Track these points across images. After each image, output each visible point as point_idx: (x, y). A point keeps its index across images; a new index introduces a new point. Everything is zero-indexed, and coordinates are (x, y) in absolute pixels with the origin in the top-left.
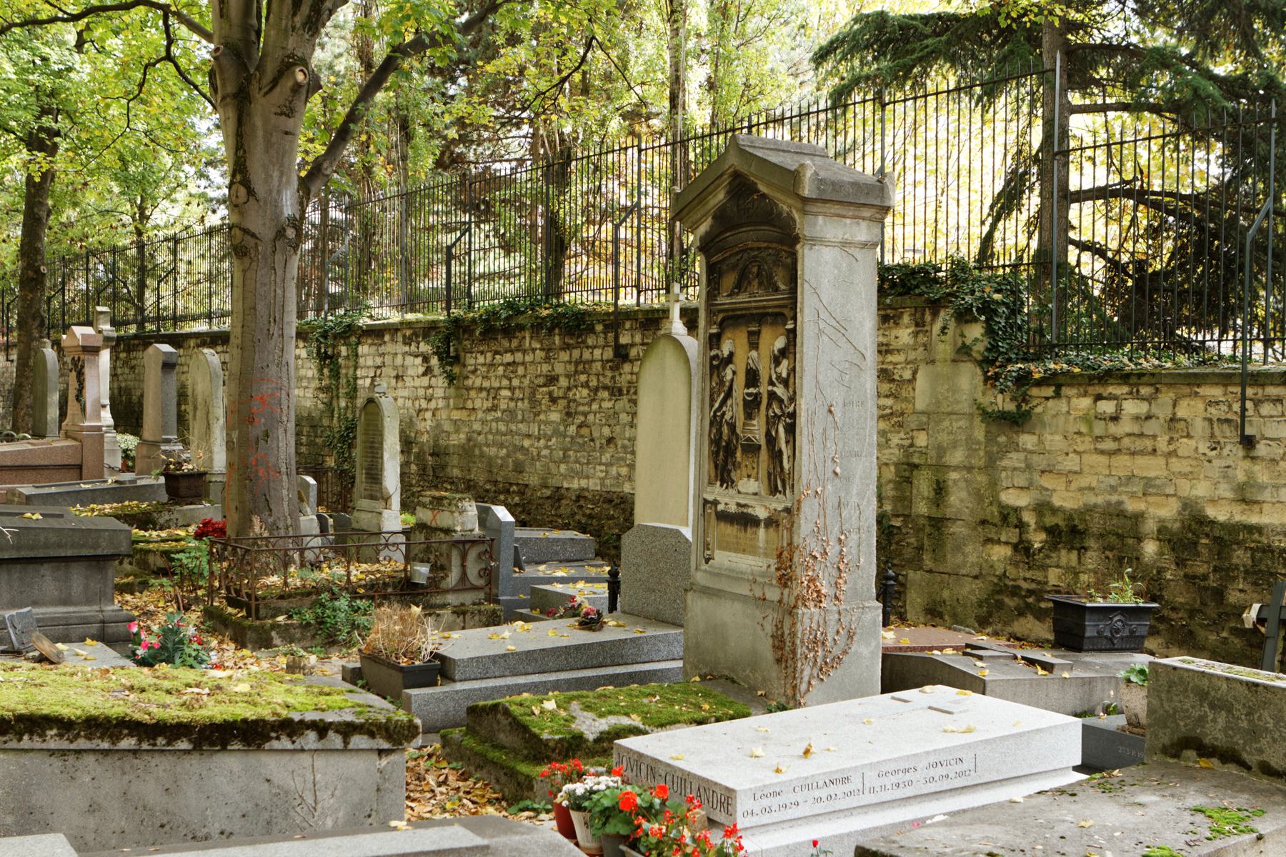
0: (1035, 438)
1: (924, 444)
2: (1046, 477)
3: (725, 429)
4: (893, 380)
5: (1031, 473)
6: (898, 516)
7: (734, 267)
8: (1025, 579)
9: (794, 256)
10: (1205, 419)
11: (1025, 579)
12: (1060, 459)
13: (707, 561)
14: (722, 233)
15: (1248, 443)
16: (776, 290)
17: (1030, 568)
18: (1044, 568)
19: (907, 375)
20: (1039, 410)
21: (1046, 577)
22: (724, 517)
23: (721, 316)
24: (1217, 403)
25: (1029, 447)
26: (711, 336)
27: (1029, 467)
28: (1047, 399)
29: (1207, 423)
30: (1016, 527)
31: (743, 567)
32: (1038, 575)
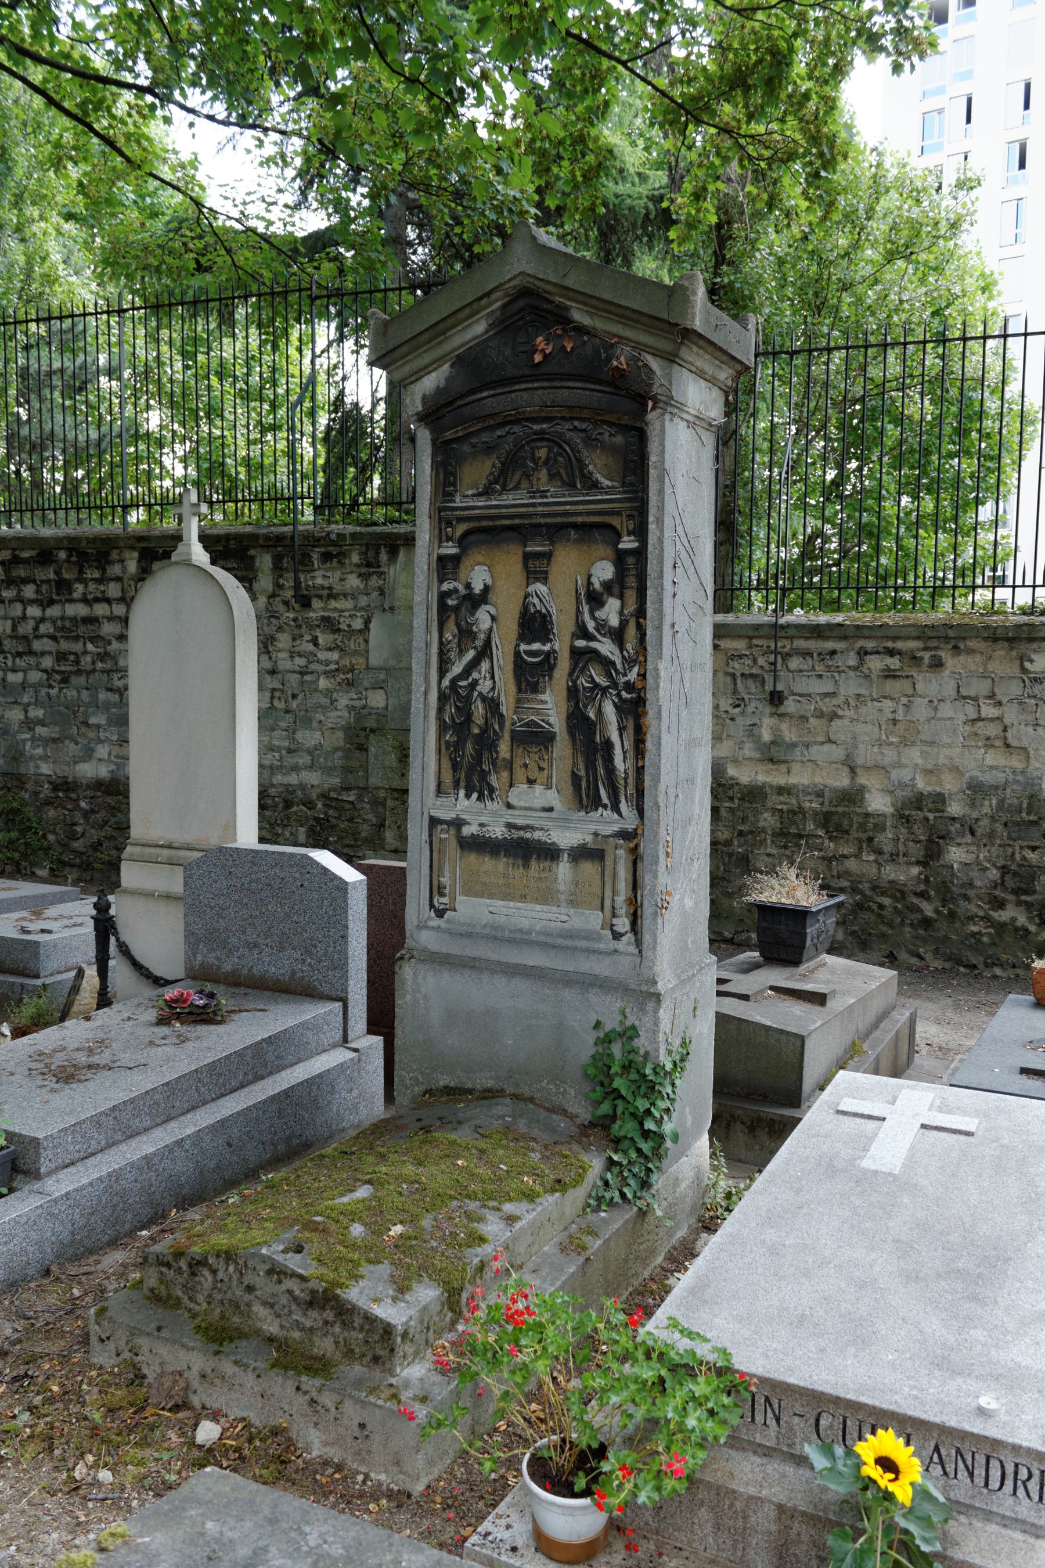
1: (382, 704)
3: (479, 710)
4: (339, 630)
6: (348, 789)
7: (489, 449)
9: (641, 437)
10: (727, 674)
13: (440, 914)
14: (473, 391)
15: (776, 698)
16: (595, 485)
19: (358, 624)
22: (479, 845)
23: (461, 529)
24: (740, 657)
26: (441, 559)
29: (729, 679)
31: (525, 924)
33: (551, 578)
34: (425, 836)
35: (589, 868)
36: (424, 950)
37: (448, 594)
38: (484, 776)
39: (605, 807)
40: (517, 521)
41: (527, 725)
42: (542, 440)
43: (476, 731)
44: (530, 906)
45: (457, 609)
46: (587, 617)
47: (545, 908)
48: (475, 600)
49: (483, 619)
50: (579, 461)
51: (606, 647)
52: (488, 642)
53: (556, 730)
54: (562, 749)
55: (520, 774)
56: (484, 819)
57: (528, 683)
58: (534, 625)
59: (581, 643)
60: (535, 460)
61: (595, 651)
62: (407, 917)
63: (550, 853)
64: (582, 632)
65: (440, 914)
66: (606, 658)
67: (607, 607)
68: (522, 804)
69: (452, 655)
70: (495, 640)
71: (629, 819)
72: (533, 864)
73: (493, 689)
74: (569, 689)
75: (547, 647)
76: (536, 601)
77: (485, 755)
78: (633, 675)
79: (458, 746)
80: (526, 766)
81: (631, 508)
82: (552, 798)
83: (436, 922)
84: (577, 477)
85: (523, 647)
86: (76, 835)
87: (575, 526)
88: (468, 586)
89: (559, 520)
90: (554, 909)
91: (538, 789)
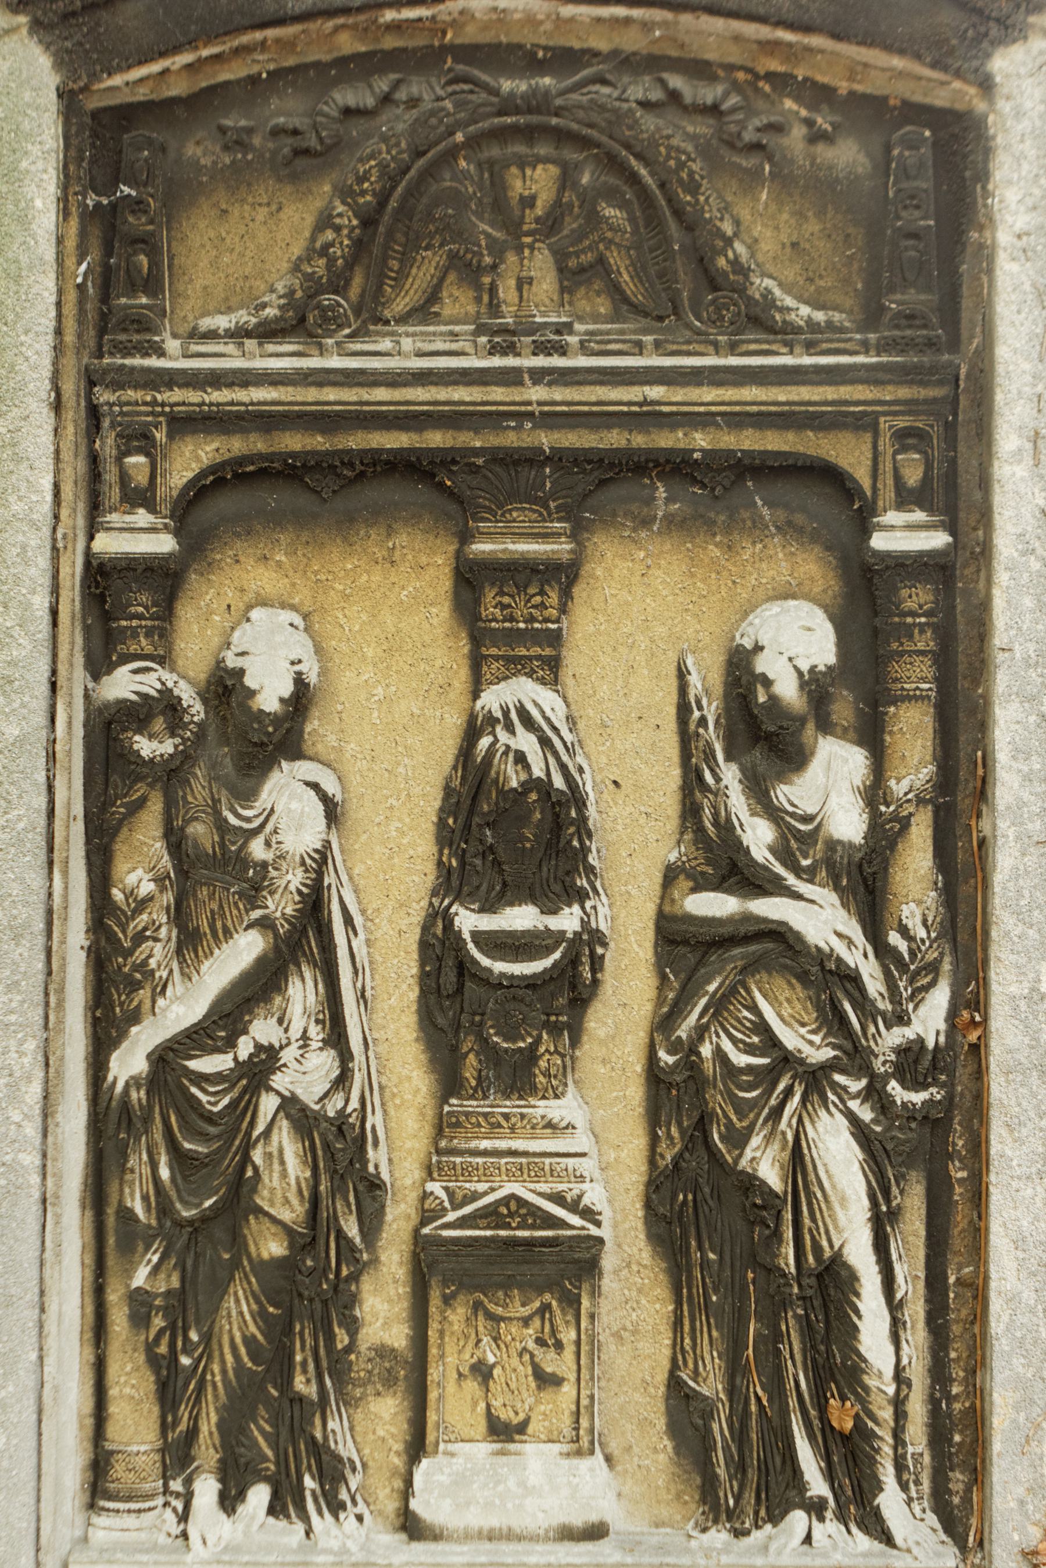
3: (283, 1170)
7: (301, 158)
16: (761, 321)
23: (189, 460)
26: (104, 580)
33: (573, 661)
37: (138, 714)
38: (296, 1419)
39: (816, 1509)
40: (436, 439)
41: (492, 1215)
42: (528, 134)
43: (274, 1248)
45: (171, 774)
46: (738, 802)
48: (262, 738)
49: (288, 809)
50: (689, 222)
51: (821, 919)
52: (314, 904)
53: (604, 1232)
54: (633, 1299)
55: (456, 1404)
57: (491, 1055)
58: (510, 830)
59: (715, 905)
60: (498, 205)
61: (780, 935)
64: (735, 872)
66: (822, 958)
67: (816, 768)
68: (476, 1519)
69: (158, 954)
70: (343, 893)
73: (342, 1081)
74: (655, 1077)
75: (568, 921)
76: (526, 742)
77: (303, 1331)
78: (930, 1019)
79: (186, 1308)
80: (482, 1372)
81: (911, 406)
82: (587, 1488)
84: (689, 283)
85: (468, 921)
87: (678, 467)
88: (225, 688)
89: (614, 439)
91: (537, 1457)
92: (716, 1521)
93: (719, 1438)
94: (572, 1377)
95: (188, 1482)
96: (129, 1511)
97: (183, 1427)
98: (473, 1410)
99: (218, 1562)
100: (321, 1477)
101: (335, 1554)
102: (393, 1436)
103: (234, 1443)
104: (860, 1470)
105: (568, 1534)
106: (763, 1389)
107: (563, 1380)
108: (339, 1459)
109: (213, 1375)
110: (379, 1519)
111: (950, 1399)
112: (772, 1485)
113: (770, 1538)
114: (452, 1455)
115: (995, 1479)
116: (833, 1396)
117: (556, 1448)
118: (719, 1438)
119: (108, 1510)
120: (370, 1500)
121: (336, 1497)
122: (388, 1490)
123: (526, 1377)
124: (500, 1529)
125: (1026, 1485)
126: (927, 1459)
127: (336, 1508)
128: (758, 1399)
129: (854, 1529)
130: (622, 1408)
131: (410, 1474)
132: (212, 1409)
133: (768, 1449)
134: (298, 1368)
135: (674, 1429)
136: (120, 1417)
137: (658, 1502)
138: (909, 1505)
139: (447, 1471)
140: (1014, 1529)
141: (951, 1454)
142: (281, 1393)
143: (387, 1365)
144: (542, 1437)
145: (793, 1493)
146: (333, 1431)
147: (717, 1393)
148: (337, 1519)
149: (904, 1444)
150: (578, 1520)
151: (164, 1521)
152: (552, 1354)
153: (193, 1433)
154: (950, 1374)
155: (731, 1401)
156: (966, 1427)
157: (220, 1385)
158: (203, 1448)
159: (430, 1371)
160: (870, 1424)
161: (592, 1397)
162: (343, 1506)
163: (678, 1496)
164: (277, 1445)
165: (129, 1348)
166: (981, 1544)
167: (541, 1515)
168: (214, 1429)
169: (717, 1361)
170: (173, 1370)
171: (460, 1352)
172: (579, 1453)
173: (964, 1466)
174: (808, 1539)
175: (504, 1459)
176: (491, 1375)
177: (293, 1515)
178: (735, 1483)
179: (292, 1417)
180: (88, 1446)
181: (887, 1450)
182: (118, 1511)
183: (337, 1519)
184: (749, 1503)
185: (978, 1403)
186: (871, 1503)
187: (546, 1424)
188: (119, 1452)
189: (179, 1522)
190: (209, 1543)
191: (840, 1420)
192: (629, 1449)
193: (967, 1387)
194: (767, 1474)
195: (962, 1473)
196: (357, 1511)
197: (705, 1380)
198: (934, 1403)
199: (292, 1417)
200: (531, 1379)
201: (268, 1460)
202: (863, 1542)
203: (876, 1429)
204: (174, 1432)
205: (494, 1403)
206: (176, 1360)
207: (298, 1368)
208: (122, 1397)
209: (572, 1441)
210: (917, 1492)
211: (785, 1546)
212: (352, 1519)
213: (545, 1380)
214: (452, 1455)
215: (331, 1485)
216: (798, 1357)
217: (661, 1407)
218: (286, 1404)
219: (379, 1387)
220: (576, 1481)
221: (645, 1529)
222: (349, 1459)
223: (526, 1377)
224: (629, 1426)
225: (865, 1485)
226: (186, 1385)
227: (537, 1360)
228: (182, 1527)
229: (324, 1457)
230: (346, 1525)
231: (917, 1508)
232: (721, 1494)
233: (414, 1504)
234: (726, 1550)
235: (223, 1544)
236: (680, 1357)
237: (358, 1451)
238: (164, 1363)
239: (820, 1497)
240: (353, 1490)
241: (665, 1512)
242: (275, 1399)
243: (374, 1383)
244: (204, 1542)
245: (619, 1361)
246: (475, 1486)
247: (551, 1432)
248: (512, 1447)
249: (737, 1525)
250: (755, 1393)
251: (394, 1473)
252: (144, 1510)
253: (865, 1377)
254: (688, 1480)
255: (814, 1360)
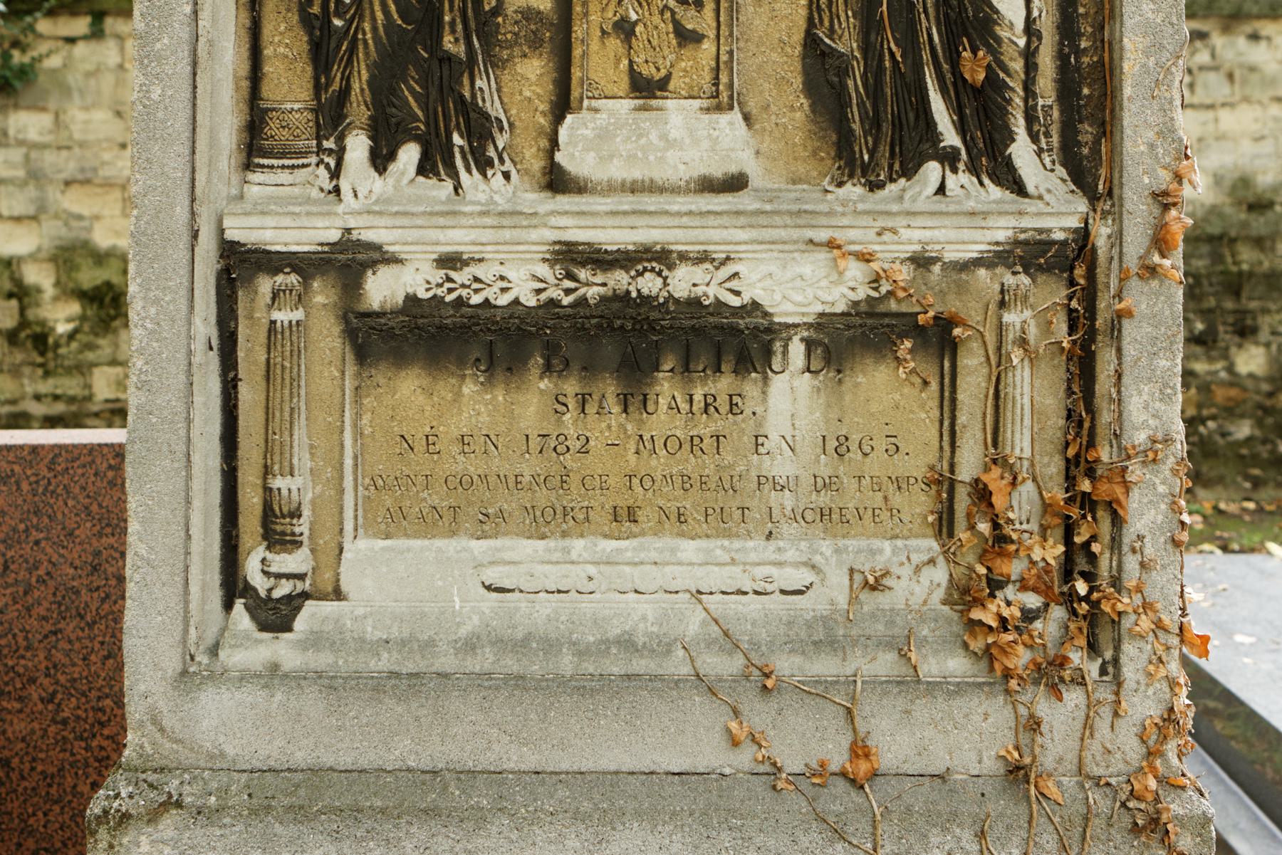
0: (46, 120)
2: (75, 191)
5: (40, 187)
8: (38, 397)
11: (38, 397)
12: (107, 156)
13: (276, 616)
17: (47, 374)
18: (82, 369)
20: (54, 62)
21: (88, 386)
22: (448, 335)
25: (33, 135)
27: (35, 176)
28: (71, 40)
30: (10, 296)
31: (641, 615)
32: (70, 386)
34: (205, 326)
35: (888, 391)
36: (218, 764)
38: (446, 78)
39: (949, 159)
44: (654, 546)
47: (718, 547)
55: (600, 61)
56: (457, 239)
62: (132, 645)
63: (734, 342)
65: (276, 616)
68: (618, 171)
71: (1056, 209)
72: (666, 388)
80: (625, 29)
82: (724, 141)
83: (251, 648)
86: (1222, 300)
90: (755, 548)
91: (678, 114)
92: (851, 176)
93: (854, 95)
94: (712, 34)
95: (341, 139)
96: (283, 167)
97: (336, 86)
98: (616, 67)
99: (369, 212)
100: (468, 135)
101: (482, 205)
102: (539, 95)
103: (385, 102)
104: (992, 122)
105: (709, 186)
106: (896, 45)
107: (703, 36)
108: (487, 117)
109: (364, 33)
110: (526, 178)
111: (1079, 53)
112: (906, 139)
113: (904, 190)
114: (596, 110)
115: (1125, 123)
116: (965, 49)
117: (697, 103)
118: (854, 95)
119: (263, 166)
120: (517, 160)
121: (484, 154)
122: (534, 150)
123: (667, 34)
124: (643, 181)
125: (1156, 129)
126: (1056, 114)
127: (484, 165)
128: (892, 54)
129: (986, 181)
130: (760, 67)
131: (556, 133)
132: (363, 66)
133: (902, 105)
134: (447, 27)
135: (810, 88)
136: (275, 76)
137: (795, 159)
138: (1039, 156)
139: (591, 125)
140: (1145, 173)
141: (1080, 107)
142: (431, 55)
143: (533, 27)
144: (683, 93)
145: (927, 145)
146: (481, 89)
147: (852, 51)
148: (485, 175)
149: (1034, 96)
150: (717, 171)
151: (317, 176)
152: (692, 12)
153: (345, 92)
154: (1079, 28)
155: (865, 59)
156: (1095, 81)
157: (370, 42)
158: (355, 105)
159: (575, 28)
160: (1002, 75)
161: (731, 53)
162: (490, 163)
163: (814, 153)
164: (427, 105)
165: (282, 9)
166: (1110, 194)
167: (682, 167)
168: (365, 87)
169: (851, 20)
170: (326, 32)
171: (603, 10)
172: (719, 108)
173: (1092, 119)
174: (941, 190)
175: (647, 114)
176: (633, 33)
177: (442, 172)
178: (869, 138)
179: (441, 78)
180: (244, 107)
181: (1018, 101)
182: (272, 167)
183: (485, 175)
184: (883, 155)
185: (1106, 55)
186: (1002, 153)
187: (687, 80)
188: (274, 109)
189: (331, 179)
190: (360, 195)
191: (973, 71)
192: (766, 108)
193: (1094, 42)
194: (901, 129)
195: (1091, 126)
196: (504, 169)
197: (840, 37)
198: (1062, 58)
199: (441, 78)
200: (672, 36)
201: (420, 121)
202: (995, 192)
203: (1008, 80)
204: (326, 92)
205: (636, 59)
206: (330, 22)
207: (447, 27)
208: (276, 56)
209: (713, 97)
210: (1047, 143)
211: (920, 193)
212: (499, 176)
213: (687, 37)
214: (596, 110)
215: (479, 143)
216: (931, 11)
217: (798, 66)
218: (435, 64)
219: (525, 48)
220: (717, 133)
221: (783, 186)
222: (497, 119)
223: (667, 34)
224: (766, 85)
225: (997, 136)
226: (339, 47)
227: (677, 17)
228: (334, 183)
229: (472, 115)
230: (493, 181)
231: (1047, 160)
232: (857, 149)
233: (559, 157)
234: (862, 199)
235: (374, 198)
236: (816, 16)
237: (505, 112)
238: (317, 24)
239: (952, 147)
240: (500, 148)
241: (801, 169)
242: (425, 60)
243: (521, 45)
244: (356, 196)
245: (757, 22)
246: (618, 140)
247: (691, 88)
248: (654, 102)
249: (872, 178)
250: (890, 49)
251: (541, 131)
252: (298, 167)
253: (997, 28)
254: (824, 137)
255: (946, 15)
